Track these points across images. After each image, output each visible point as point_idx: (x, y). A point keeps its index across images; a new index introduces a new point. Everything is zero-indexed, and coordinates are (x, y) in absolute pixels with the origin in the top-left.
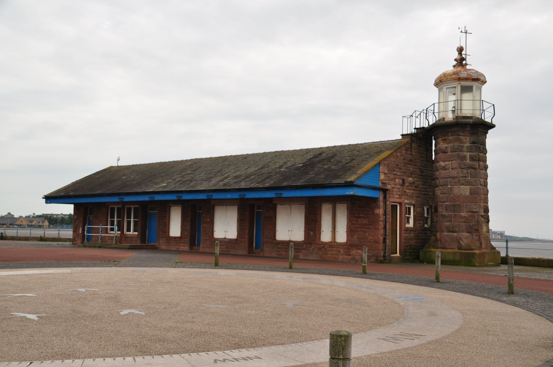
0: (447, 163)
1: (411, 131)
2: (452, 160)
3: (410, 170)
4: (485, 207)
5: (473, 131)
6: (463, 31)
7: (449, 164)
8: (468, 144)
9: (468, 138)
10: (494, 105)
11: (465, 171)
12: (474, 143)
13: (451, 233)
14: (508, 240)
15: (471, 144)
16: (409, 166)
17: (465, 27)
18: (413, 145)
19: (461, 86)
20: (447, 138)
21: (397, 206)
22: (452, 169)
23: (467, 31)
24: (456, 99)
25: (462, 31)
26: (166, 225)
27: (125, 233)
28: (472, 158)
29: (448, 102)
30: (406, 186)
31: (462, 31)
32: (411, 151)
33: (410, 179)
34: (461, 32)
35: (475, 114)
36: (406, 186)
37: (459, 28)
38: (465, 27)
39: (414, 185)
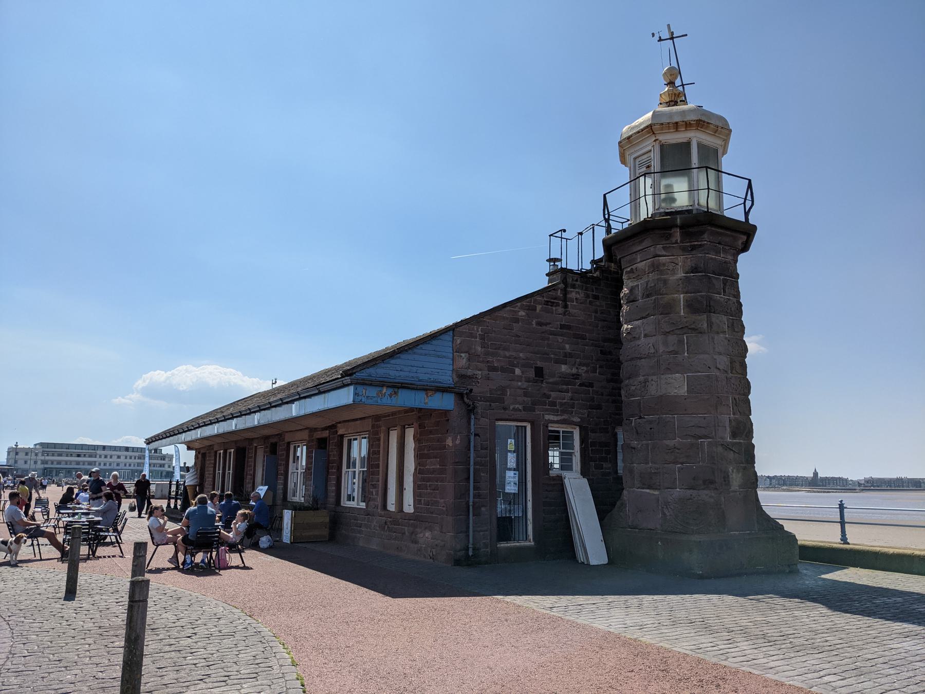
0: (636, 323)
1: (580, 268)
2: (644, 316)
3: (564, 348)
4: (734, 424)
5: (690, 242)
6: (666, 35)
7: (639, 327)
8: (681, 274)
9: (680, 259)
10: (750, 181)
11: (672, 339)
12: (695, 270)
13: (648, 491)
14: (843, 502)
15: (687, 273)
16: (560, 339)
17: (669, 26)
18: (573, 295)
19: (662, 147)
20: (634, 267)
21: (525, 427)
22: (646, 336)
23: (672, 33)
24: (711, 209)
25: (660, 37)
26: (916, 487)
27: (135, 500)
28: (692, 307)
29: (631, 182)
30: (547, 383)
31: (660, 37)
32: (566, 306)
33: (564, 368)
34: (660, 40)
35: (698, 204)
36: (547, 383)
37: (653, 35)
38: (669, 26)
39: (578, 382)
